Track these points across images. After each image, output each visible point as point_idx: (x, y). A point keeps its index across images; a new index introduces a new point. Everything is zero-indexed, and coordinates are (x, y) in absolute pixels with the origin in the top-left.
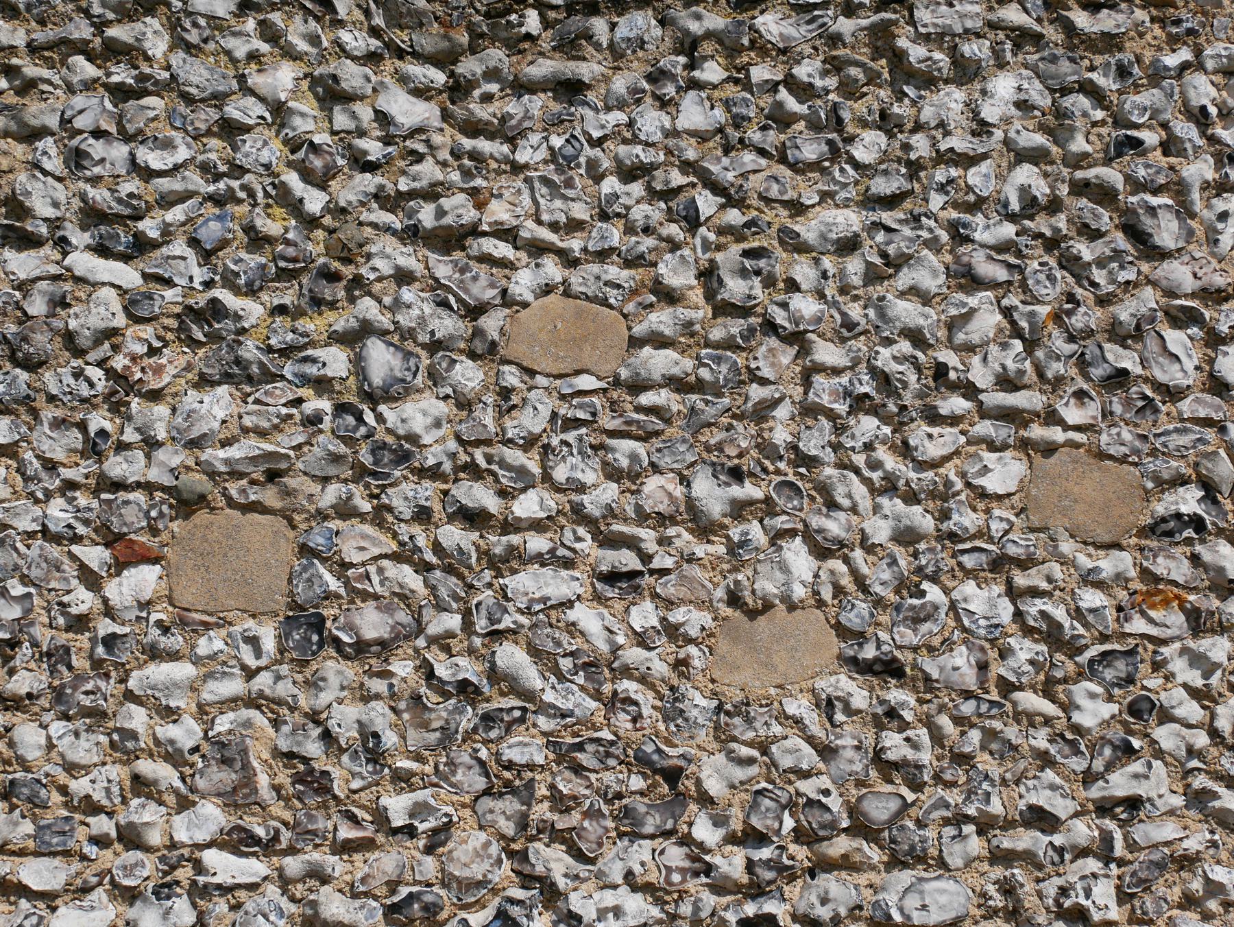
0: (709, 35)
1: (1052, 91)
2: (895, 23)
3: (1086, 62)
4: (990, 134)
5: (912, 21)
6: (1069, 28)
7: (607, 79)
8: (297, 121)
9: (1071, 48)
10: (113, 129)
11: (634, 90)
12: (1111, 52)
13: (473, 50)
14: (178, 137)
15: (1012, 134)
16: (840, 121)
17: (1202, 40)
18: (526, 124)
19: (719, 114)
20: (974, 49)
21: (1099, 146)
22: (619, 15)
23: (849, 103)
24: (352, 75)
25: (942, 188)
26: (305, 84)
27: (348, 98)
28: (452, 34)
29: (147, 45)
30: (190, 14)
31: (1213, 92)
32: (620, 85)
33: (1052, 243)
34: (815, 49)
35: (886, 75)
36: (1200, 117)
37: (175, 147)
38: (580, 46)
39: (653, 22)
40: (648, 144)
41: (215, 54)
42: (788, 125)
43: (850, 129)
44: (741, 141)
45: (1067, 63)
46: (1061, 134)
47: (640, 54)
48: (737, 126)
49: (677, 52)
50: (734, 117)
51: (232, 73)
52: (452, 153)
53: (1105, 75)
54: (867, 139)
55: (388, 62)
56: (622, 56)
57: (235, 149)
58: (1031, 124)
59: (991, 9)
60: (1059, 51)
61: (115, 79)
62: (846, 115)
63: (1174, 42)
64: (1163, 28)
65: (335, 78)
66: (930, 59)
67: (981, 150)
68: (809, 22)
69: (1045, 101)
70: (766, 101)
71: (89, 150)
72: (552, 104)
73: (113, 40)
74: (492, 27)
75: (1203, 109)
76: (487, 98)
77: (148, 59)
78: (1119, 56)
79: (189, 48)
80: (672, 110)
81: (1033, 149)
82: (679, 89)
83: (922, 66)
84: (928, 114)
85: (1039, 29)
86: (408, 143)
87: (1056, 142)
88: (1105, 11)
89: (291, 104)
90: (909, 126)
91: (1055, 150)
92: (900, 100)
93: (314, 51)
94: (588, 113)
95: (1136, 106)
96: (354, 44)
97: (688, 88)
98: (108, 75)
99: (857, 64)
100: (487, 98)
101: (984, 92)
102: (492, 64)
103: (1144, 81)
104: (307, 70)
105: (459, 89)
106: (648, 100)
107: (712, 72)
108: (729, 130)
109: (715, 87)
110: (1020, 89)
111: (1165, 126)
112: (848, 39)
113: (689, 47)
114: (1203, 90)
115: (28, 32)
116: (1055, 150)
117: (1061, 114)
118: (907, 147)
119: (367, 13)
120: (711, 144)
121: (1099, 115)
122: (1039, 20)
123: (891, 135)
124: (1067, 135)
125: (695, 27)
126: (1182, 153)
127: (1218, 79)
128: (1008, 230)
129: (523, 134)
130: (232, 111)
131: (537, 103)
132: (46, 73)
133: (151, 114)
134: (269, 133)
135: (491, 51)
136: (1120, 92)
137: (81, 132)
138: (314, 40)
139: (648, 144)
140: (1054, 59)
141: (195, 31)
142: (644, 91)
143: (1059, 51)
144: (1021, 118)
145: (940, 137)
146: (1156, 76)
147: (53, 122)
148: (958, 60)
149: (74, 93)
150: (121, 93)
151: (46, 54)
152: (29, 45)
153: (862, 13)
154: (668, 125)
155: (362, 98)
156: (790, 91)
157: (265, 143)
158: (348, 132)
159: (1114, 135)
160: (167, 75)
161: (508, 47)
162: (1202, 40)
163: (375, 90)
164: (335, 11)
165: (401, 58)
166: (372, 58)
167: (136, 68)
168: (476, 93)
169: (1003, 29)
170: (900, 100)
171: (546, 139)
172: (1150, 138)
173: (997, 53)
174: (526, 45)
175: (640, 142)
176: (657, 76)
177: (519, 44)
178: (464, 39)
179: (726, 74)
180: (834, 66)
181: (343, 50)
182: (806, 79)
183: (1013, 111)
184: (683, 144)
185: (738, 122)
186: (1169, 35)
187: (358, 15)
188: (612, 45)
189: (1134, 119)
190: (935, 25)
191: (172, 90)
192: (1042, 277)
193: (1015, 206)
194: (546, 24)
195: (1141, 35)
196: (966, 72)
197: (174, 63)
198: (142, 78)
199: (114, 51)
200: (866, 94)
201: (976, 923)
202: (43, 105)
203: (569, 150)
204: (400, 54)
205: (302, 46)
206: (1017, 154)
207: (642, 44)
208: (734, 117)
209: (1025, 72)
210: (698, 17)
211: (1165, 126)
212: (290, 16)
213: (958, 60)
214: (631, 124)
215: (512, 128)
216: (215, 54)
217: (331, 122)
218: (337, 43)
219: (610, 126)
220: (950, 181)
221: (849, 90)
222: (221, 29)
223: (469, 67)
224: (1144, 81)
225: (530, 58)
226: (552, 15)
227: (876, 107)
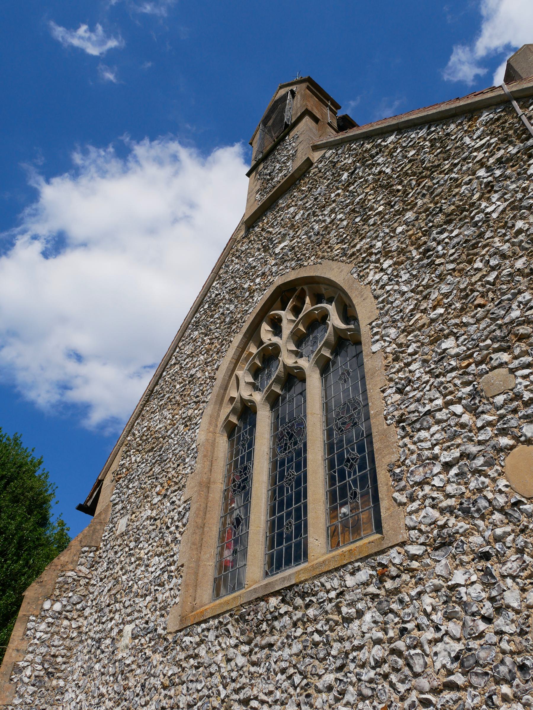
25: (353, 661)
33: (386, 676)
83: (347, 616)
95: (405, 614)
110: (372, 617)
121: (397, 620)
127: (434, 594)
128: (372, 674)
134: (218, 674)
162: (425, 581)
192: (382, 691)
193: (373, 664)
195: (407, 585)
201: (270, 706)
220: (355, 658)
226: (269, 622)
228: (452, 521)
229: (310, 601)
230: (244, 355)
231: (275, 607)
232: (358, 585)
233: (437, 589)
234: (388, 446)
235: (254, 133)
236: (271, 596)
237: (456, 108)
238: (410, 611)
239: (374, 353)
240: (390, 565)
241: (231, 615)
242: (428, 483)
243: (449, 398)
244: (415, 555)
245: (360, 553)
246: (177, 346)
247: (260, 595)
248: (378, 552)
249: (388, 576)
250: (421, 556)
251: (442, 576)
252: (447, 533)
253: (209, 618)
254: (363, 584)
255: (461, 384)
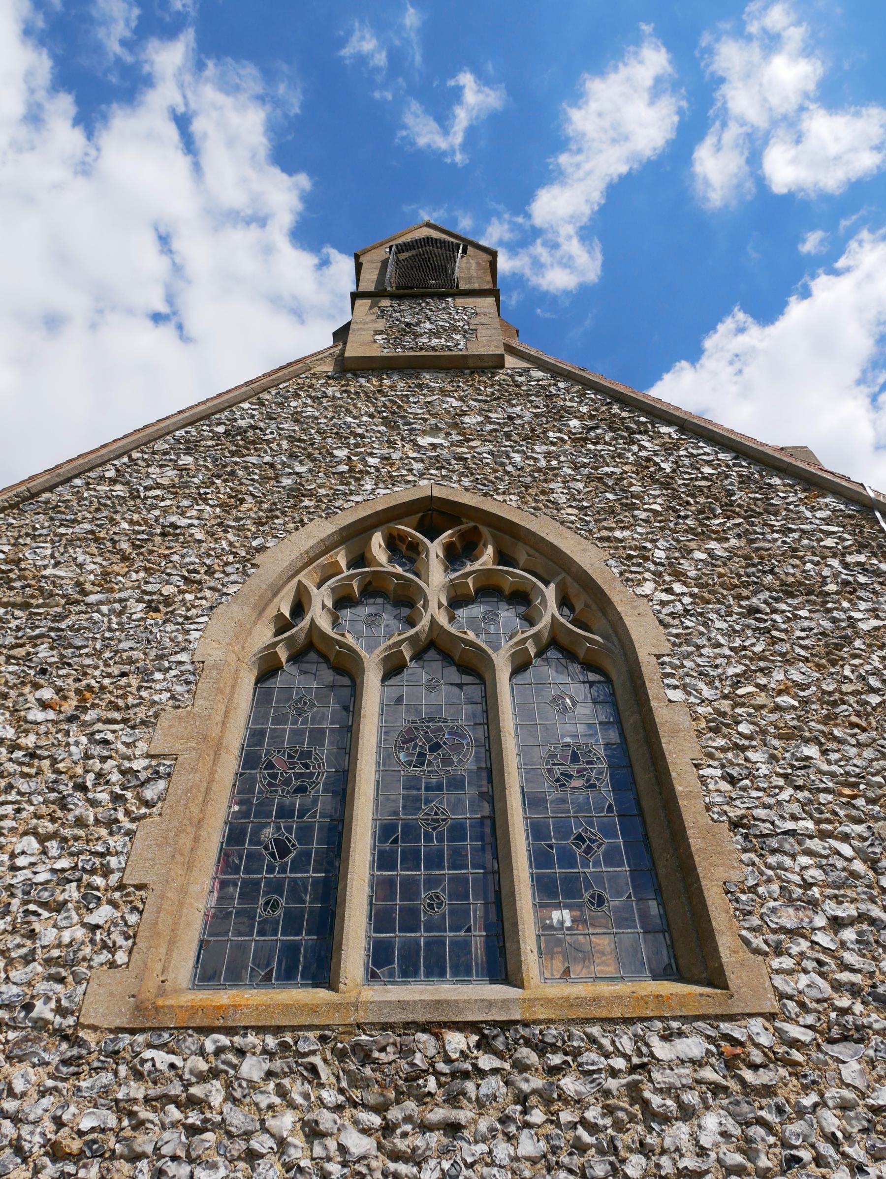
0: (534, 1092)
1: (741, 1124)
2: (641, 1082)
3: (757, 1104)
4: (708, 1156)
5: (651, 1080)
6: (742, 1081)
7: (475, 1122)
8: (292, 1151)
9: (747, 1095)
10: (183, 1154)
11: (492, 1129)
12: (770, 1097)
13: (398, 1102)
14: (220, 1160)
15: (721, 1155)
16: (616, 1148)
17: (822, 1087)
18: (428, 1153)
19: (543, 1145)
20: (691, 1098)
21: (776, 1163)
22: (482, 1079)
23: (620, 1135)
24: (326, 1120)
26: (299, 1125)
27: (323, 1135)
28: (385, 1092)
29: (211, 1099)
30: (238, 1079)
31: (837, 1122)
32: (483, 1126)
34: (596, 1099)
35: (640, 1116)
36: (832, 1139)
37: (218, 1168)
38: (459, 1101)
39: (502, 1084)
40: (500, 1167)
41: (249, 1105)
42: (585, 1151)
43: (623, 1154)
44: (557, 1163)
45: (746, 1105)
46: (752, 1154)
47: (494, 1104)
48: (554, 1153)
49: (516, 1103)
50: (552, 1147)
51: (257, 1118)
52: (383, 1173)
53: (770, 1113)
54: (634, 1161)
55: (347, 1110)
56: (484, 1106)
57: (253, 1169)
58: (732, 1147)
59: (695, 1071)
60: (740, 1097)
61: (190, 1121)
62: (619, 1144)
63: (806, 1088)
64: (798, 1079)
65: (316, 1122)
66: (664, 1105)
67: (704, 1168)
68: (591, 1082)
69: (737, 1131)
70: (570, 1135)
71: (167, 1170)
72: (443, 1138)
73: (193, 1095)
74: (409, 1087)
75: (833, 1134)
76: (405, 1135)
77: (210, 1108)
78: (776, 1099)
79: (235, 1101)
80: (514, 1142)
81: (736, 1166)
82: (518, 1128)
83: (661, 1110)
84: (668, 1143)
85: (724, 1082)
86: (356, 1166)
87: (749, 1160)
88: (762, 1070)
89: (290, 1139)
90: (658, 1151)
91: (749, 1165)
92: (650, 1133)
93: (305, 1103)
94: (465, 1145)
95: (793, 1133)
96: (329, 1099)
97: (524, 1127)
98: (186, 1118)
99: (622, 1109)
100: (405, 1135)
101: (700, 1126)
102: (408, 1112)
103: (794, 1115)
104: (301, 1116)
105: (388, 1129)
106: (500, 1136)
107: (537, 1116)
108: (549, 1156)
109: (539, 1126)
110: (721, 1124)
111: (813, 1146)
112: (615, 1093)
113: (522, 1099)
114: (831, 1121)
115: (146, 1089)
116: (749, 1165)
117: (749, 1140)
118: (658, 1166)
119: (338, 1078)
120: (539, 1166)
121: (772, 1140)
122: (724, 1077)
123: (648, 1158)
124: (754, 1155)
125: (525, 1087)
126: (827, 1165)
127: (838, 1112)
129: (425, 1160)
130: (255, 1144)
131: (435, 1138)
132: (151, 1116)
133: (207, 1145)
134: (274, 1158)
135: (407, 1103)
136: (782, 1124)
137: (164, 1157)
138: (306, 1096)
139: (500, 1167)
140: (737, 1103)
141: (239, 1090)
142: (497, 1130)
143: (740, 1097)
144: (725, 1143)
145: (677, 1158)
146: (801, 1112)
147: (149, 1149)
148: (681, 1105)
149: (165, 1129)
150: (193, 1130)
151: (154, 1103)
152: (145, 1097)
153: (621, 1075)
154: (512, 1154)
155: (331, 1135)
156: (584, 1128)
157: (272, 1166)
158: (321, 1159)
159: (784, 1153)
160: (219, 1118)
161: (418, 1100)
162: (822, 1087)
163: (339, 1130)
164: (319, 1077)
165: (355, 1107)
166: (339, 1108)
167: (203, 1113)
168: (399, 1131)
169: (705, 1083)
170: (650, 1133)
171: (439, 1163)
172: (806, 1155)
173: (704, 1100)
174: (428, 1099)
175: (496, 1166)
176: (505, 1120)
177: (424, 1098)
178: (392, 1095)
179: (545, 1117)
180: (609, 1111)
181: (322, 1103)
182: (593, 1120)
183: (720, 1139)
184: (522, 1166)
185: (555, 1150)
186: (802, 1084)
187: (333, 1080)
188: (478, 1099)
189: (793, 1142)
190: (665, 1083)
191: (221, 1128)
194: (440, 1085)
196: (687, 1113)
197: (225, 1110)
198: (205, 1121)
199: (193, 1103)
200: (629, 1130)
202: (146, 1137)
203: (453, 1172)
204: (355, 1105)
205: (299, 1100)
206: (727, 1169)
207: (495, 1098)
208: (552, 1147)
209: (722, 1112)
210: (527, 1080)
211: (813, 1146)
212: (294, 1080)
213: (681, 1105)
214: (490, 1152)
215: (420, 1156)
216: (249, 1105)
217: (311, 1151)
218: (319, 1098)
219: (477, 1154)
221: (619, 1126)
222: (254, 1088)
223: (395, 1114)
224: (794, 1115)
225: (430, 1107)
226: (443, 1079)
227: (636, 1138)
228: (858, 1008)
229: (565, 1062)
230: (323, 560)
231: (462, 1052)
232: (682, 1061)
233: (845, 1107)
234: (720, 853)
235: (368, 247)
236: (450, 1028)
237: (790, 464)
238: (799, 1131)
239: (670, 701)
240: (748, 1043)
241: (323, 1039)
242: (804, 937)
243: (825, 826)
244: (798, 1041)
245: (682, 1006)
246: (127, 453)
247: (421, 1018)
248: (722, 1015)
249: (744, 1061)
250: (807, 1045)
251: (854, 1087)
252: (854, 1024)
253: (246, 1028)
254: (692, 1061)
255: (846, 816)
